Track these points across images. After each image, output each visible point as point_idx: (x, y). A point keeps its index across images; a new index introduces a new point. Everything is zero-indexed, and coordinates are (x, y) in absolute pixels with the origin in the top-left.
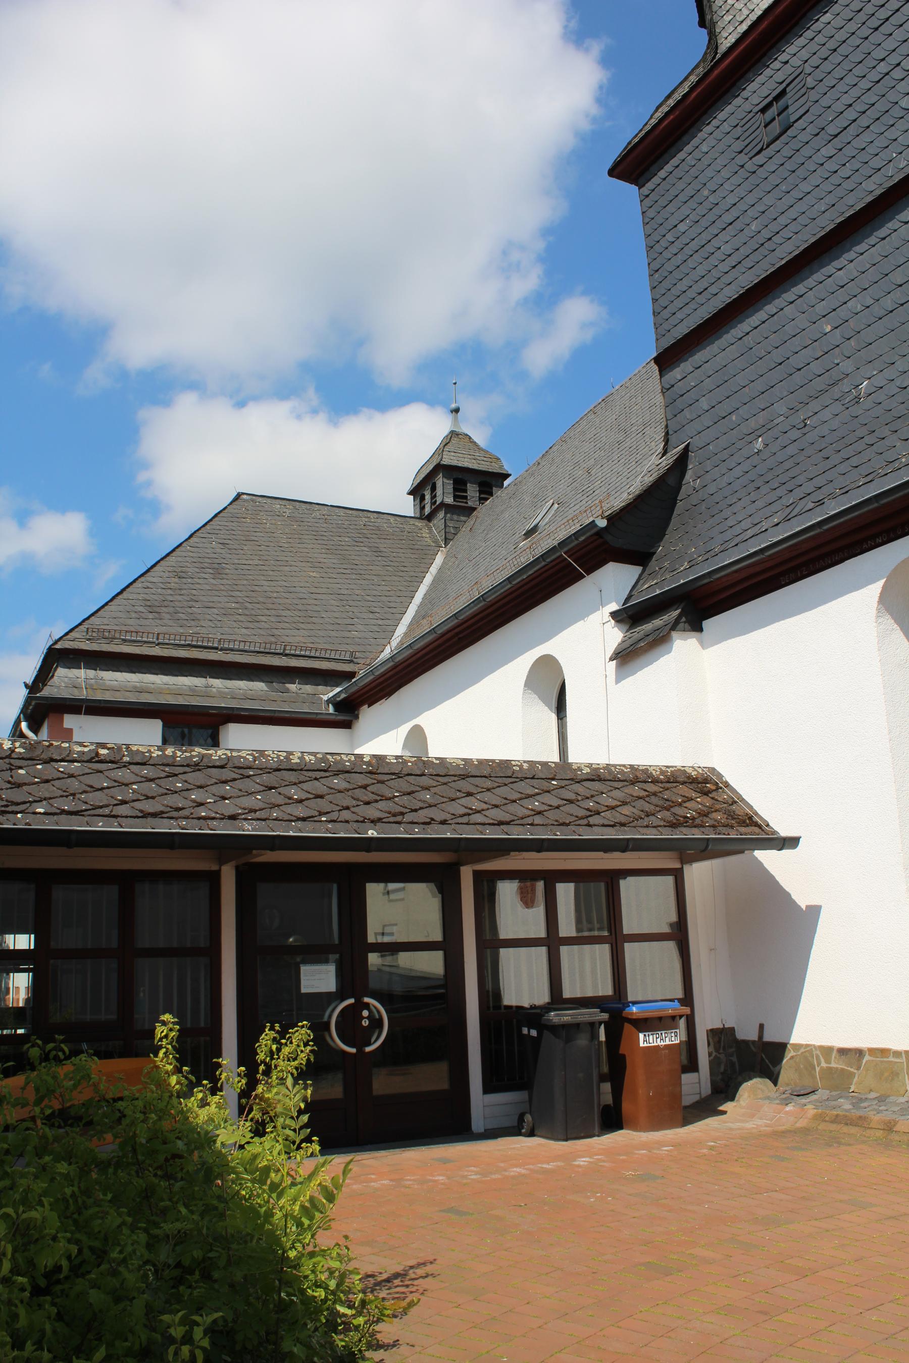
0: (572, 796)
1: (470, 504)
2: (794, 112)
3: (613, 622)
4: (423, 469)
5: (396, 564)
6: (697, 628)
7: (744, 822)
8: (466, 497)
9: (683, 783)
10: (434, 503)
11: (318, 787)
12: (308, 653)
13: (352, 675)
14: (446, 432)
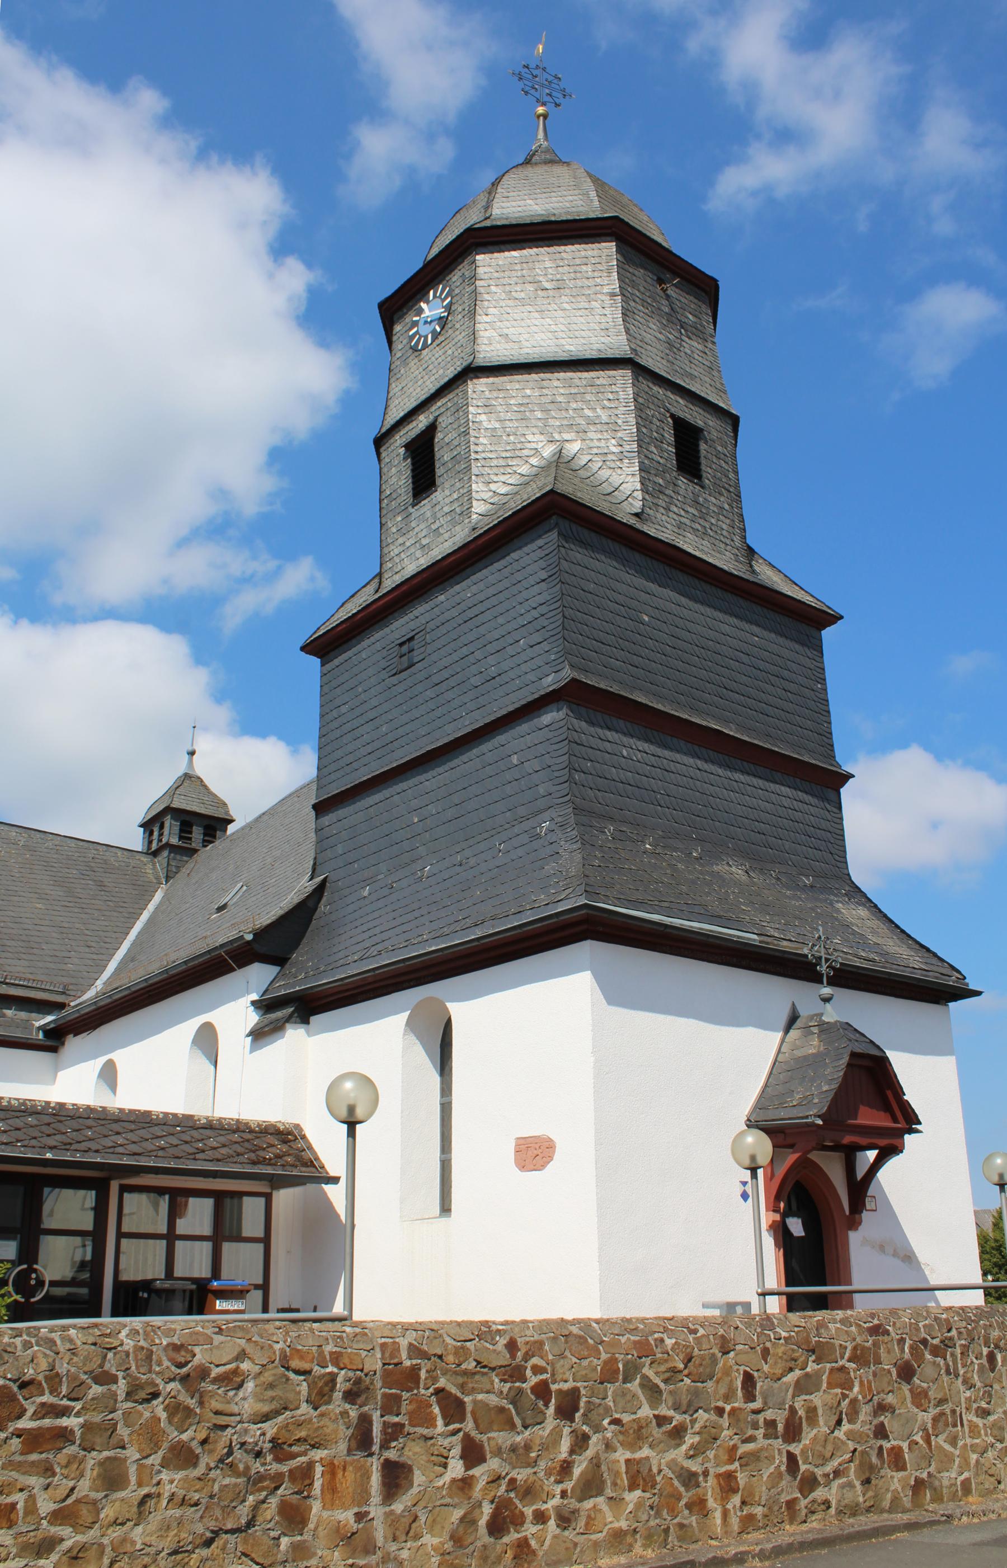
0: (188, 1138)
1: (194, 845)
2: (416, 655)
3: (253, 1008)
4: (155, 805)
5: (117, 900)
6: (305, 1021)
7: (307, 1163)
8: (190, 839)
9: (271, 1134)
10: (160, 840)
11: (18, 1123)
12: (25, 983)
13: (62, 1006)
14: (180, 772)
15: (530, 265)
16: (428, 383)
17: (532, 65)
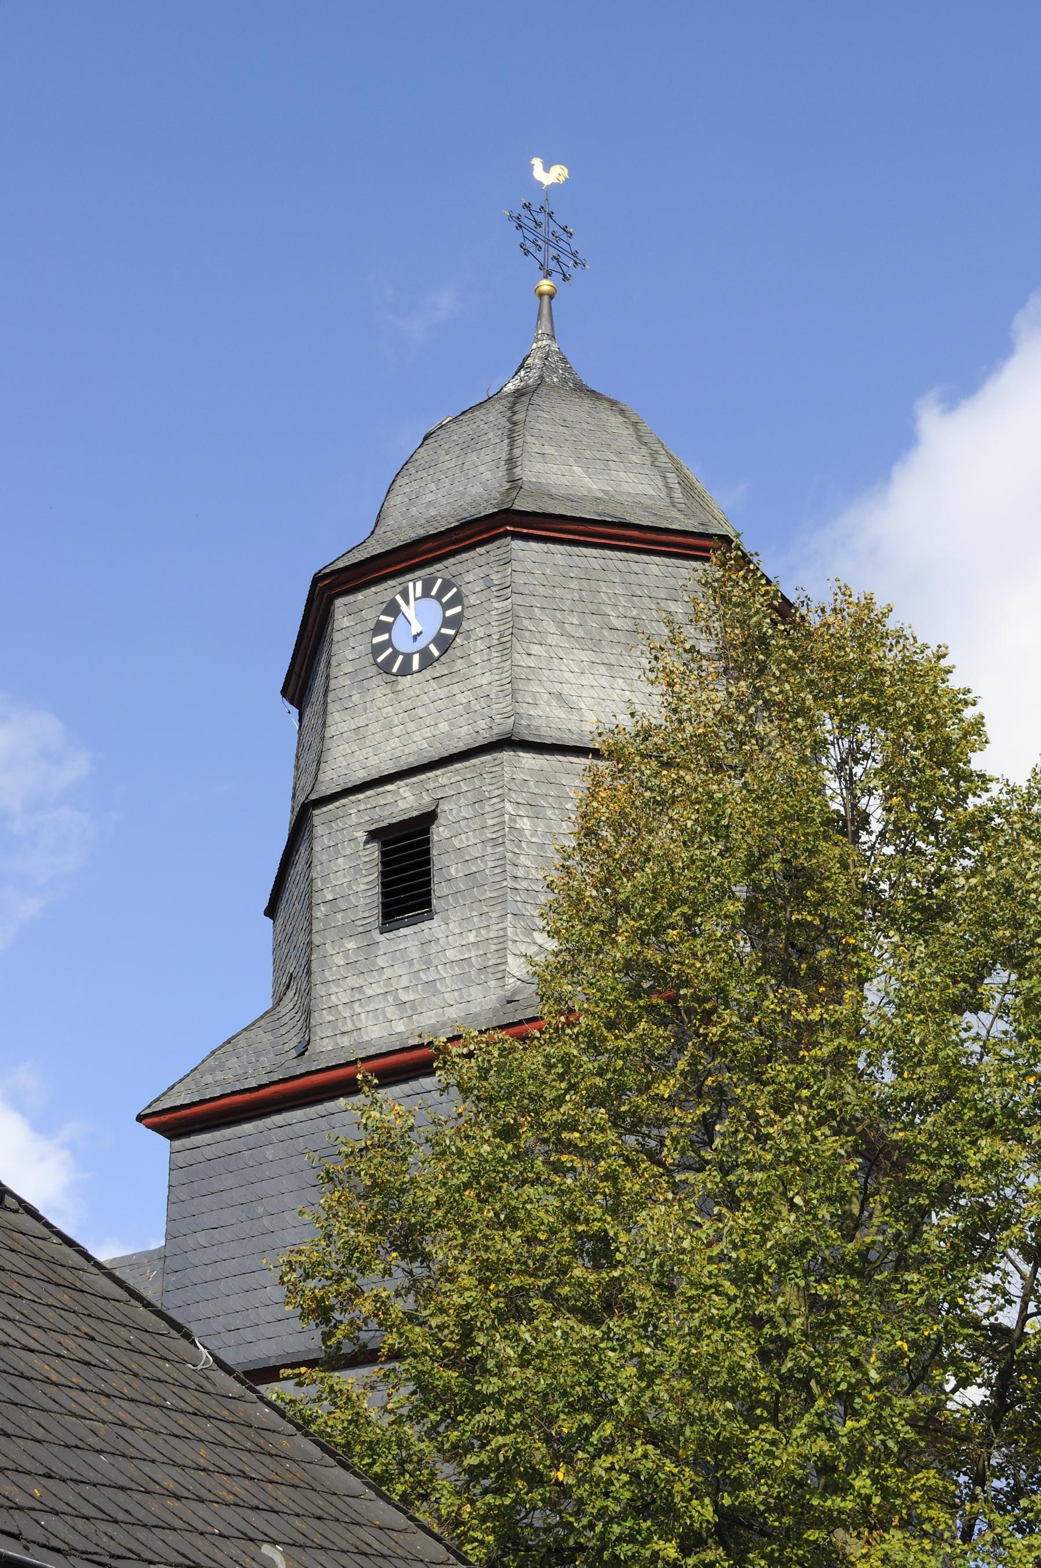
15: (594, 585)
16: (417, 736)
17: (535, 207)
